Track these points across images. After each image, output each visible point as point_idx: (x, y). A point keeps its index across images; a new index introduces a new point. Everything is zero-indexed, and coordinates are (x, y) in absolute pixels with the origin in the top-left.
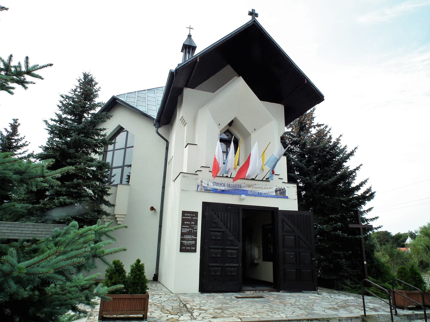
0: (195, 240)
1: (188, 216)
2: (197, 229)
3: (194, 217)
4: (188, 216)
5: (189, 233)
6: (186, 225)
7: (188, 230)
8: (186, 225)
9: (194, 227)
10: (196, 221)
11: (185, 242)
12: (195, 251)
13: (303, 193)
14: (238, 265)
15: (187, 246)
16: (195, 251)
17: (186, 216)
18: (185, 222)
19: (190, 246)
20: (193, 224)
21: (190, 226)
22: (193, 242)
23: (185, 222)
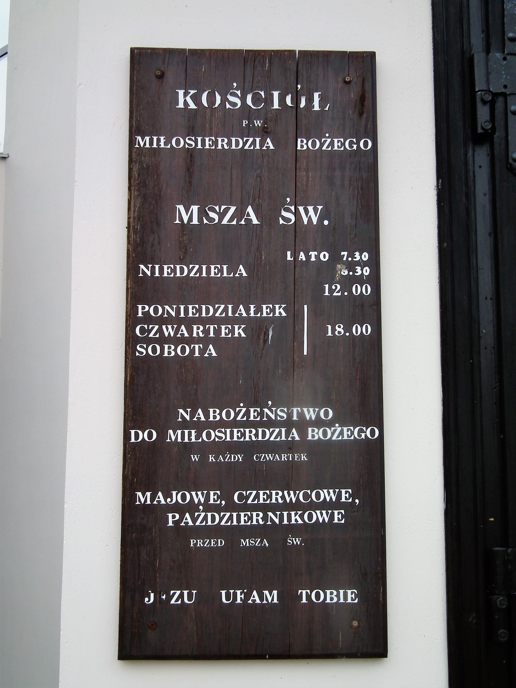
0: (366, 469)
1: (228, 123)
2: (370, 309)
3: (302, 123)
4: (228, 123)
5: (252, 372)
6: (191, 244)
7: (227, 322)
8: (191, 244)
9: (326, 272)
10: (358, 188)
11: (198, 510)
12: (369, 640)
13: (195, 458)
14: (303, 144)
15: (236, 561)
16: (369, 640)
17: (195, 123)
18: (188, 214)
19: (283, 559)
20: (298, 235)
21: (265, 264)
22: (327, 505)
23: (188, 214)
